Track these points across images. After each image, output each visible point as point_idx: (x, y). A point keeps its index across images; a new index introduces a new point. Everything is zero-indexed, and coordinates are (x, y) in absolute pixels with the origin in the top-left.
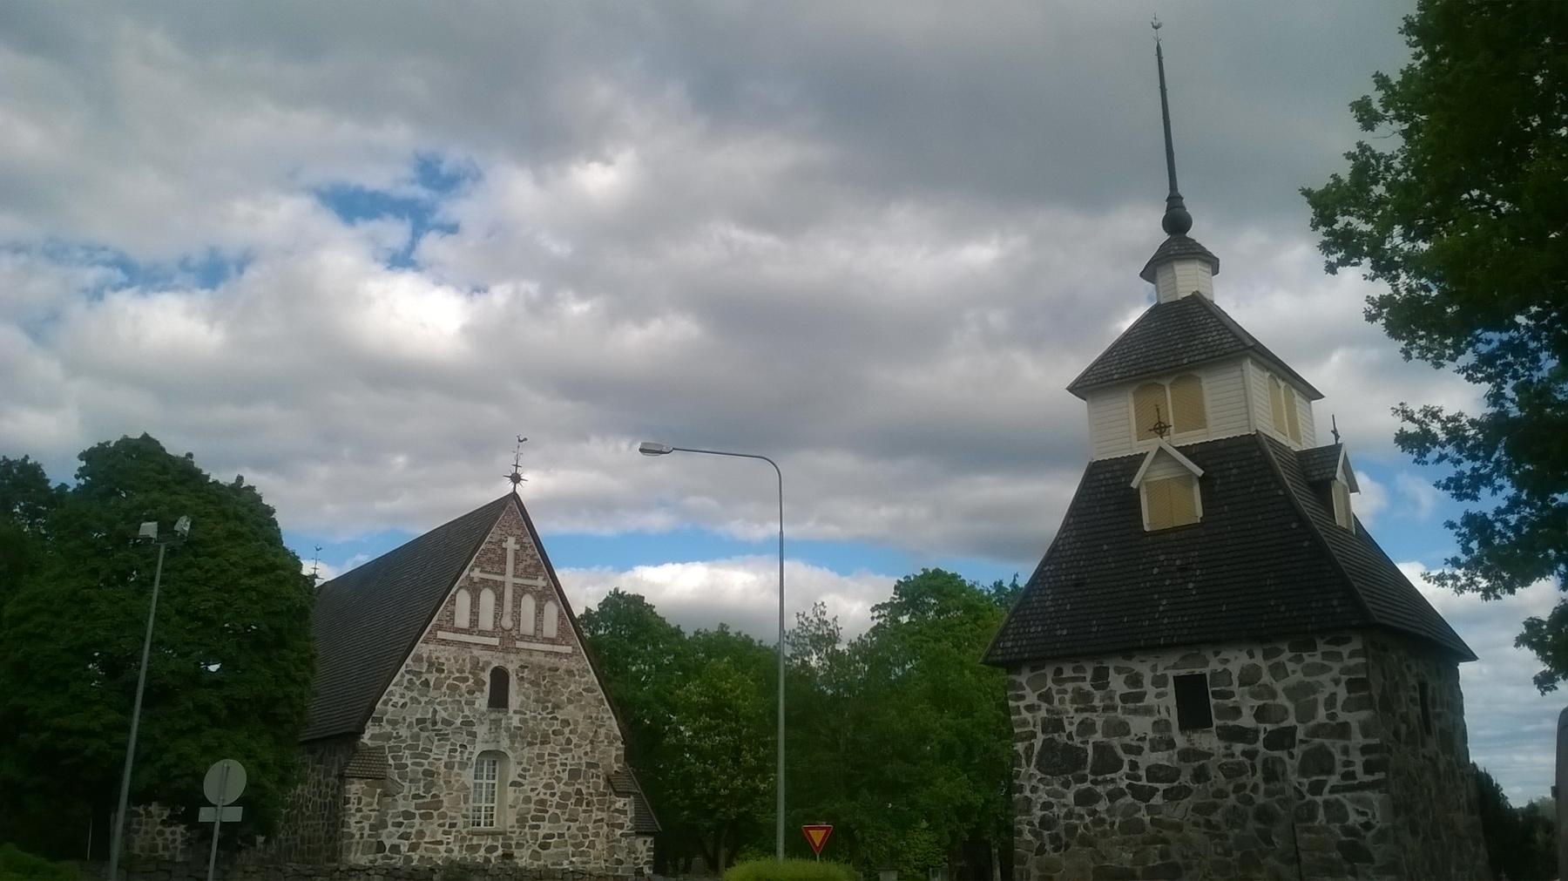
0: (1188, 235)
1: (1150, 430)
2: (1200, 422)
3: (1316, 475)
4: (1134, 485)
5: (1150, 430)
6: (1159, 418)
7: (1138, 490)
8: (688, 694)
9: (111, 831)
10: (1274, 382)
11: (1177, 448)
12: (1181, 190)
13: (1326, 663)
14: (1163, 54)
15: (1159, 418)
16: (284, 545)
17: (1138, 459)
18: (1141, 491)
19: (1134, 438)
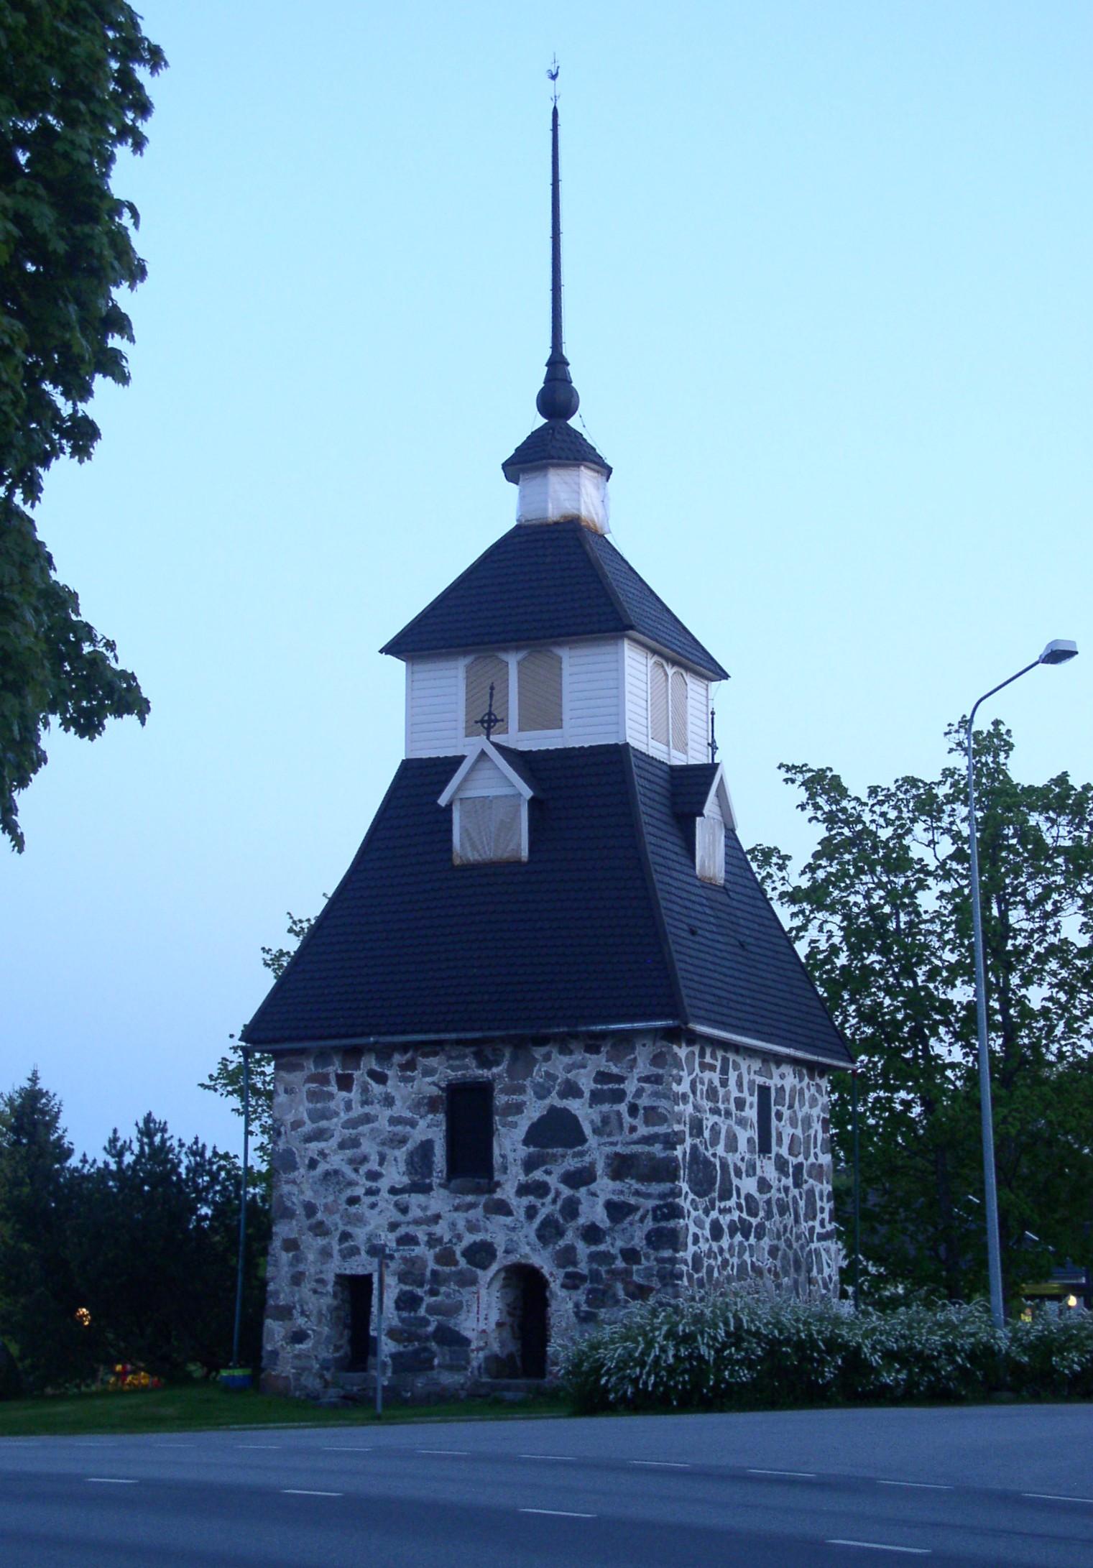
0: (569, 422)
1: (477, 722)
2: (555, 721)
3: (729, 827)
4: (443, 801)
5: (477, 722)
6: (491, 706)
7: (449, 808)
8: (840, 1213)
9: (332, 1423)
10: (661, 670)
11: (722, 778)
12: (567, 351)
13: (800, 1123)
14: (560, 121)
15: (491, 706)
16: (20, 797)
17: (454, 763)
18: (454, 808)
19: (462, 732)
